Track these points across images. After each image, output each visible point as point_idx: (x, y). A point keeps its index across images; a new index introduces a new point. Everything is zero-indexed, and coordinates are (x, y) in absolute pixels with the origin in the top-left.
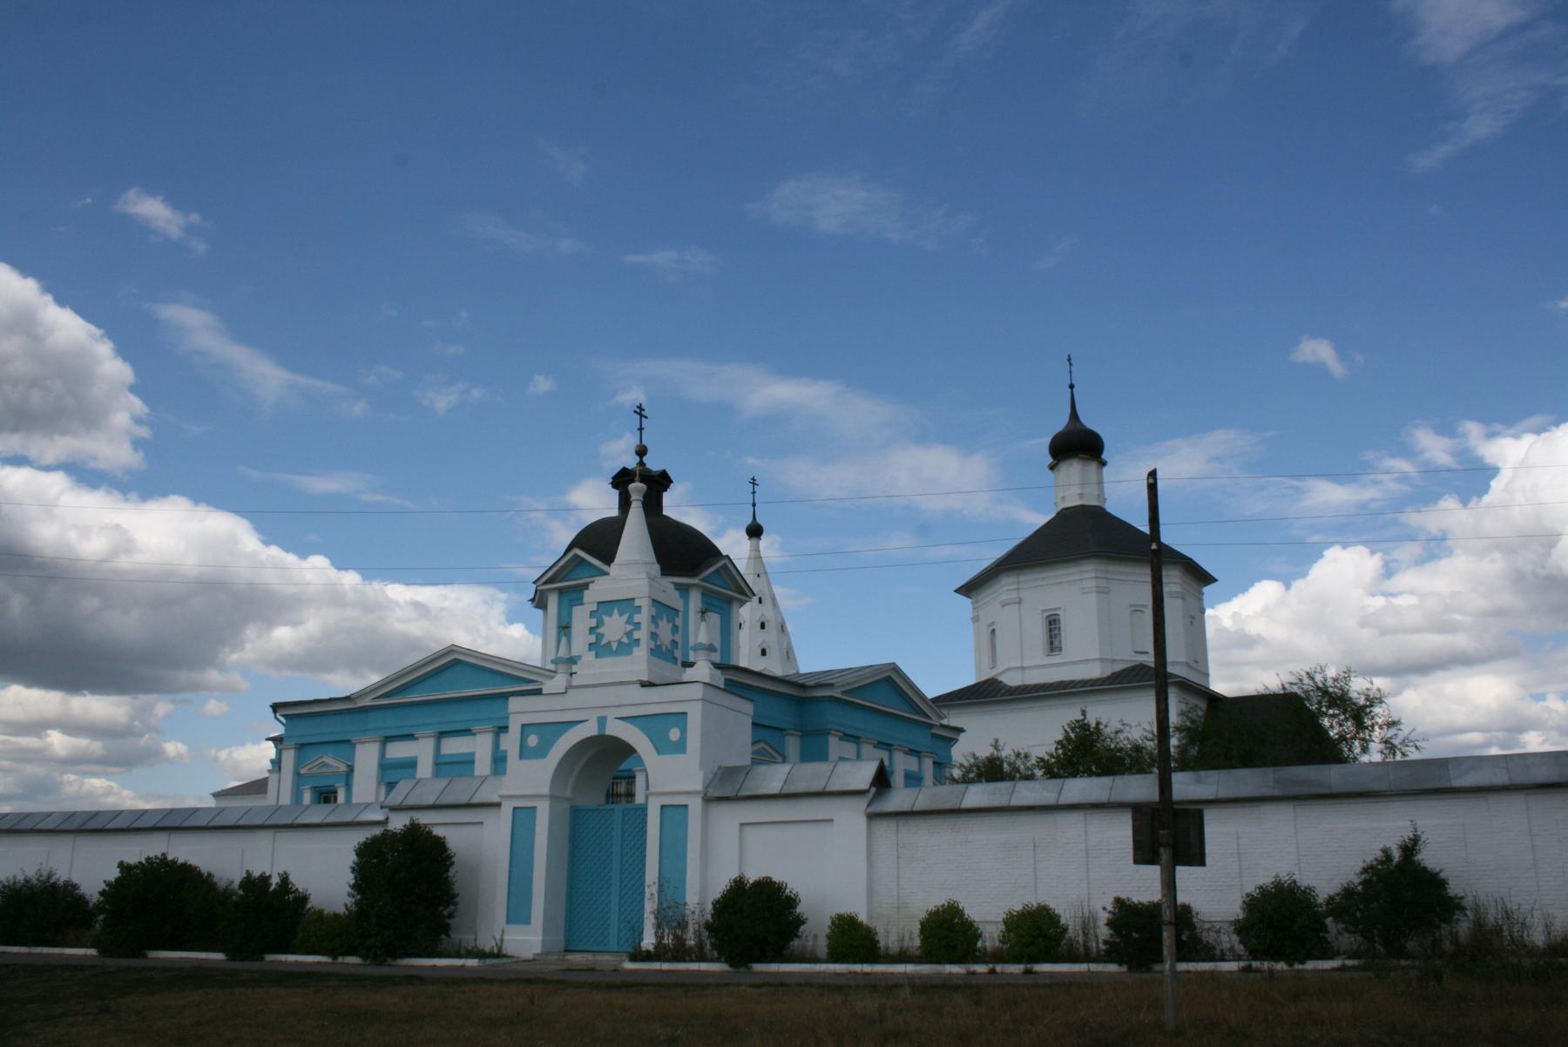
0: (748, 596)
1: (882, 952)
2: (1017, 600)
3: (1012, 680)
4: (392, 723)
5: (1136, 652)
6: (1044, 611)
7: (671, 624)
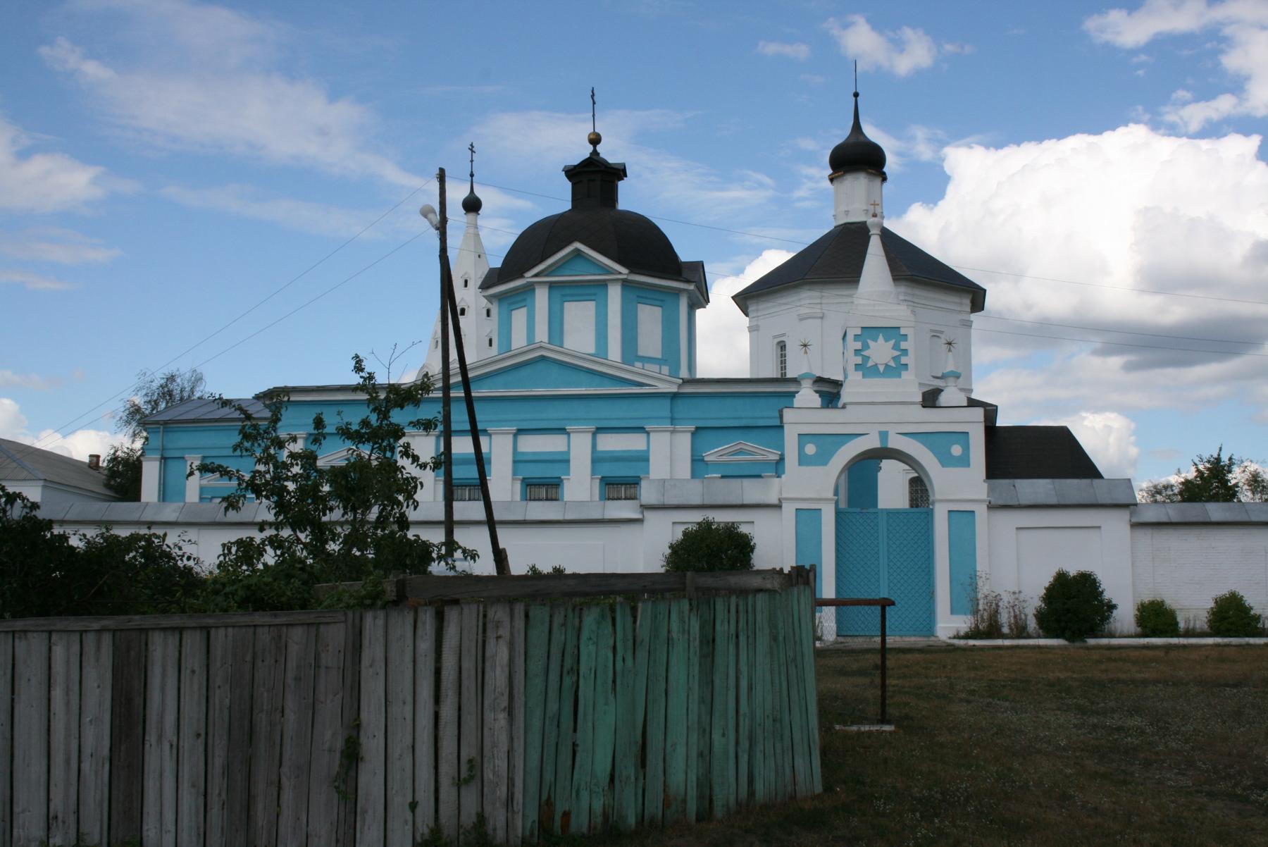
2: (821, 315)
5: (934, 377)
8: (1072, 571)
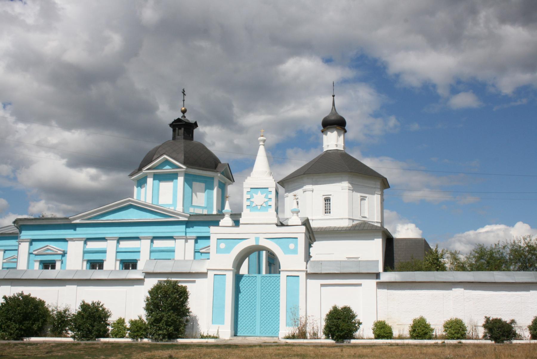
1: (437, 337)
2: (312, 190)
6: (323, 195)
8: (340, 306)
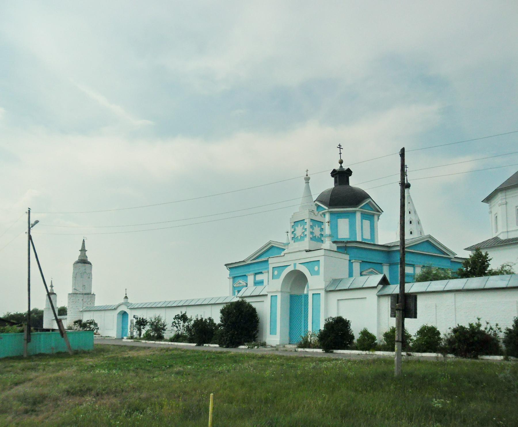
0: (380, 212)
2: (505, 203)
3: (503, 237)
4: (257, 268)
7: (320, 228)
